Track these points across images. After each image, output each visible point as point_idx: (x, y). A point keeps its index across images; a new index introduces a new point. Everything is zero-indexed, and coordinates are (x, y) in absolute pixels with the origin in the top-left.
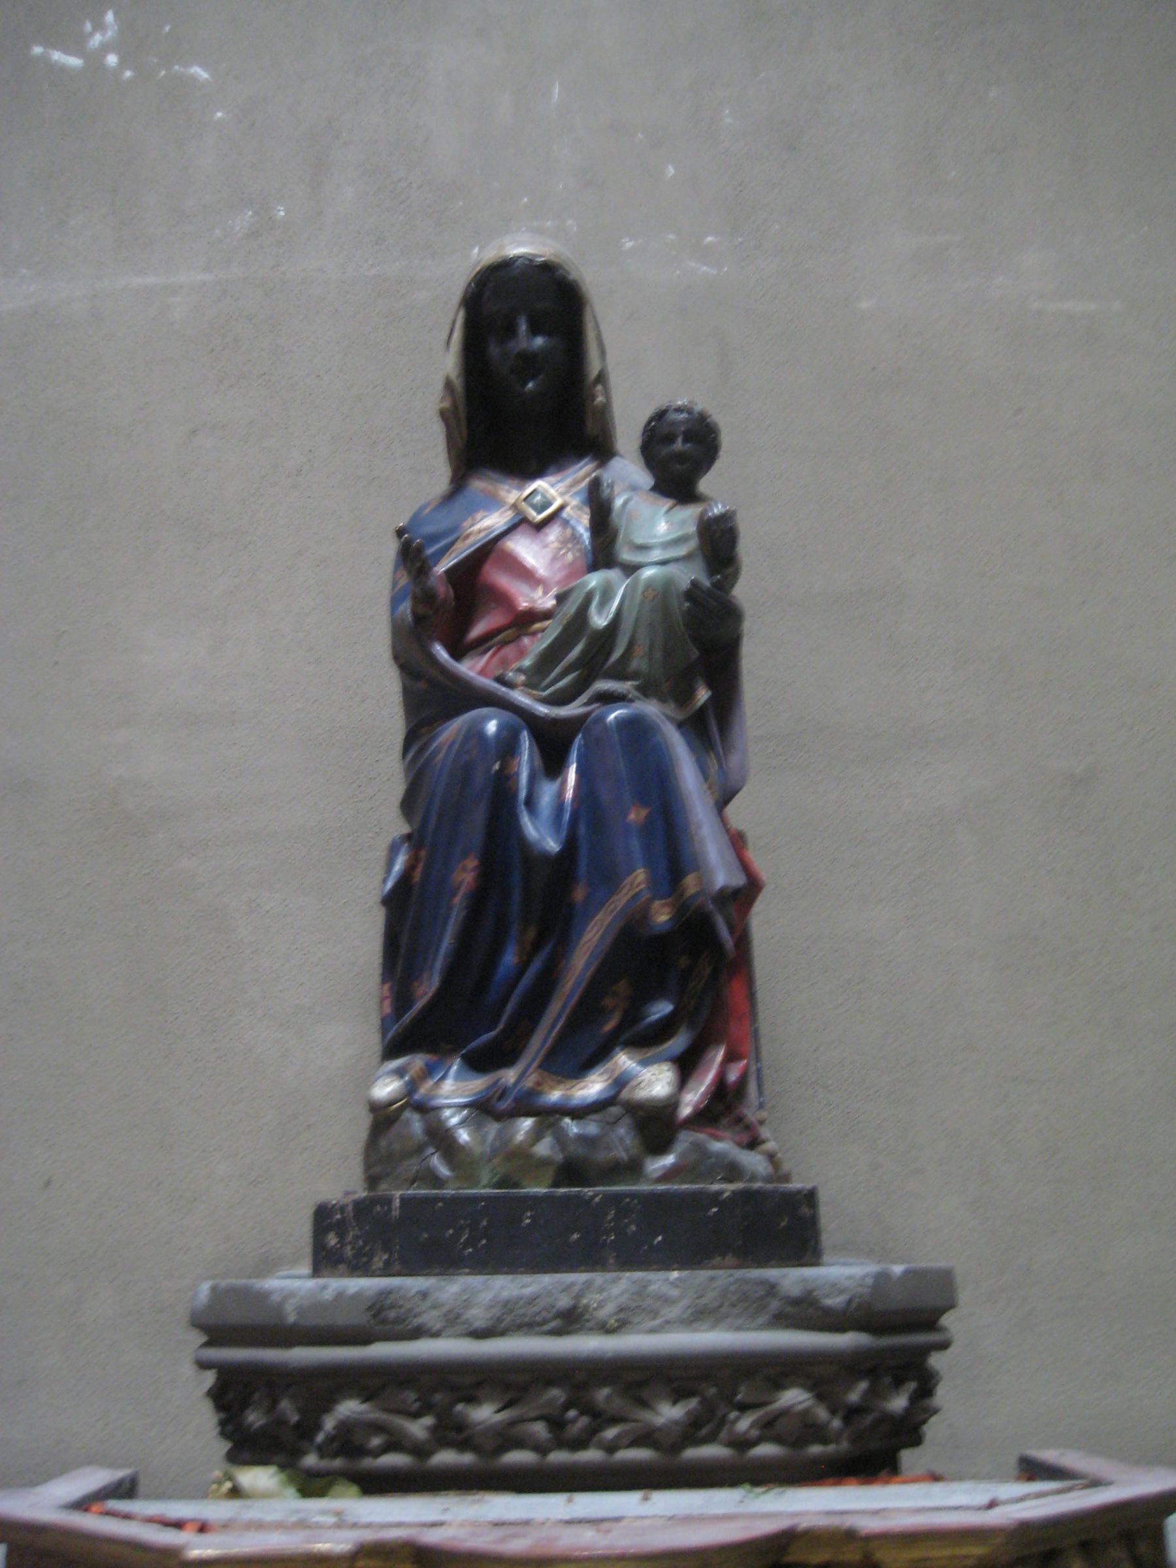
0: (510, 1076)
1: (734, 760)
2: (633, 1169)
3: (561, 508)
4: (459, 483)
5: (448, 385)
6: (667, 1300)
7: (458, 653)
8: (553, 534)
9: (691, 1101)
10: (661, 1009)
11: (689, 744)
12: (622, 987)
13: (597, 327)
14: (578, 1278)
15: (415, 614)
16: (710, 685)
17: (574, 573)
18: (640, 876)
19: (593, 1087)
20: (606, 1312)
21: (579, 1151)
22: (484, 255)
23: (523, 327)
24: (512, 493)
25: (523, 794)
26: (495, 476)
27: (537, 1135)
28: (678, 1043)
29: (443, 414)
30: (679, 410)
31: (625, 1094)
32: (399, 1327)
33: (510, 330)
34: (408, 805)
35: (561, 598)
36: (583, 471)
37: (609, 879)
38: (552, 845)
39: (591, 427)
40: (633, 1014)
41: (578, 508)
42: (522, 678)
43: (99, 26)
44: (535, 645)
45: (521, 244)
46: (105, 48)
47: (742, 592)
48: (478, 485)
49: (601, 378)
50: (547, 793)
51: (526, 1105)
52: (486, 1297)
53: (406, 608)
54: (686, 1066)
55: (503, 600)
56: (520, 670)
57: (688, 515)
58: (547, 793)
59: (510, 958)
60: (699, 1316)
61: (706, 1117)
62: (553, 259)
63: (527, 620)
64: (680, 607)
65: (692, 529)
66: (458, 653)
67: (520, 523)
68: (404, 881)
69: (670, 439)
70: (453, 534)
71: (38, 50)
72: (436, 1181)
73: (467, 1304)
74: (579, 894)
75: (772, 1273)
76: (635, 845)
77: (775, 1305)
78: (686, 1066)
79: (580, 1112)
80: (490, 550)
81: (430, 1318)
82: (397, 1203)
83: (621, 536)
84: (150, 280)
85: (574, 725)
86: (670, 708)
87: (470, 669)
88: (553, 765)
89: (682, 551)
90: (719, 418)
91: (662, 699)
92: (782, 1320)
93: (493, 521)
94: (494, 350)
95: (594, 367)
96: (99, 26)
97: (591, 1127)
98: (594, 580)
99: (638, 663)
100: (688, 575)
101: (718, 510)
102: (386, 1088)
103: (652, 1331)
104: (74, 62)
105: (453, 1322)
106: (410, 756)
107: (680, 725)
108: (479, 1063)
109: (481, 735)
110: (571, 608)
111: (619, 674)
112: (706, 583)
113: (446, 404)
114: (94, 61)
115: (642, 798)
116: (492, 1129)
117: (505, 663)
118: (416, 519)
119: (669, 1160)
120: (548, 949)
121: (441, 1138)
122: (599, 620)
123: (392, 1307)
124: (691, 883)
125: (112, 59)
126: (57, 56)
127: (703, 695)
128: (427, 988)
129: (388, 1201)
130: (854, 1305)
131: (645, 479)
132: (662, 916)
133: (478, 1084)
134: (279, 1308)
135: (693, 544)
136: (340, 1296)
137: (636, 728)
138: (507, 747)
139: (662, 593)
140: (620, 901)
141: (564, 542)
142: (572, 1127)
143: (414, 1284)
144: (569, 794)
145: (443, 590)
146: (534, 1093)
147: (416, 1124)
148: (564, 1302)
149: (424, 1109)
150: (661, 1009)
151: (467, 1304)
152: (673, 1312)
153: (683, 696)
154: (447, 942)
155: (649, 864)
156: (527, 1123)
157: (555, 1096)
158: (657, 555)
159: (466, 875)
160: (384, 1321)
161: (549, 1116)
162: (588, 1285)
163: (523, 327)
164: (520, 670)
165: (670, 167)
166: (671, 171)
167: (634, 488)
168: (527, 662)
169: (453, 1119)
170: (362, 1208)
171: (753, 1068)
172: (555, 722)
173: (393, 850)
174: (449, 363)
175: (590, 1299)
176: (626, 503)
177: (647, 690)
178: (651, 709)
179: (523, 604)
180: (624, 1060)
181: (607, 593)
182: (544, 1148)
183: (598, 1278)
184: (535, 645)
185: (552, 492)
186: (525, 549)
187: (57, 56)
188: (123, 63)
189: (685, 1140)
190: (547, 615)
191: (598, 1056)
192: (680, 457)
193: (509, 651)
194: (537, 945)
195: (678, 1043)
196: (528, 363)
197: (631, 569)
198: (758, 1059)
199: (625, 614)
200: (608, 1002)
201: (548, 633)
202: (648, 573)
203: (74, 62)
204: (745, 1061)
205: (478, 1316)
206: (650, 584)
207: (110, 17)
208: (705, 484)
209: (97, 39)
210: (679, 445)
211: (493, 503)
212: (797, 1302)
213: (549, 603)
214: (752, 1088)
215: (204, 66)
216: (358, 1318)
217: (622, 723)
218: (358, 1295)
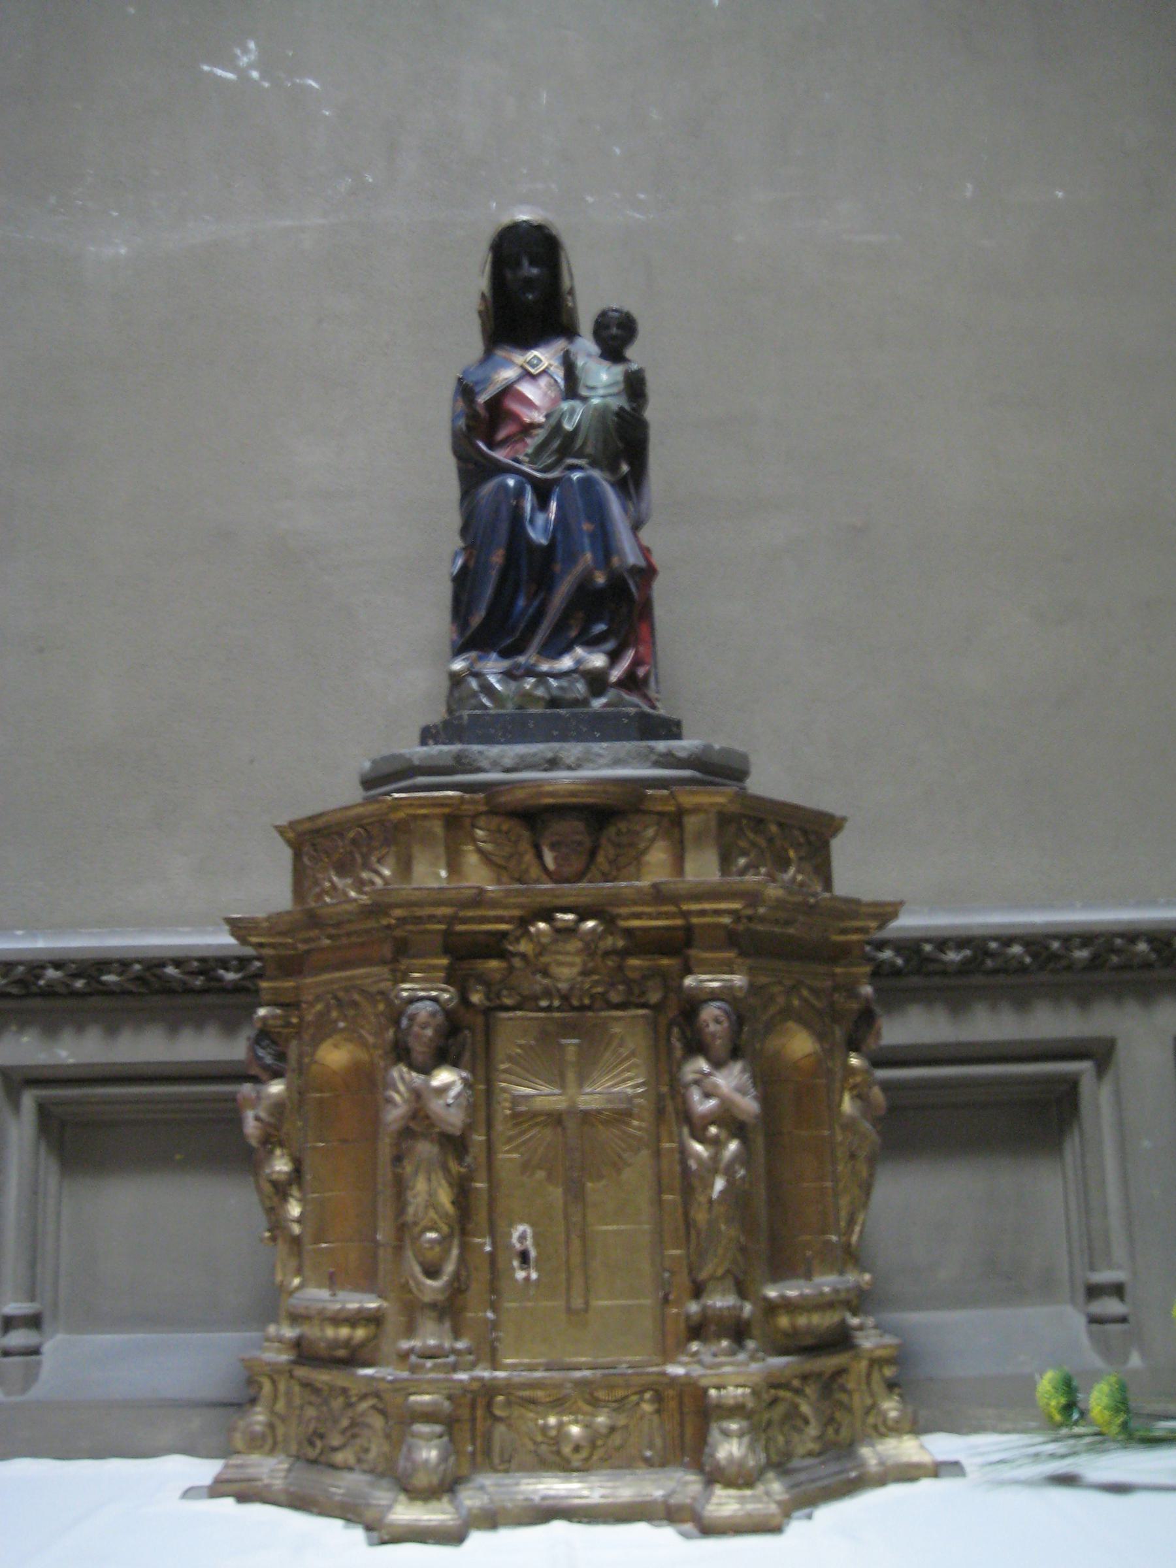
0: (521, 659)
1: (643, 506)
2: (585, 702)
3: (547, 368)
4: (488, 353)
5: (483, 295)
6: (600, 756)
7: (492, 445)
8: (543, 382)
9: (615, 675)
10: (601, 627)
11: (619, 497)
12: (581, 615)
13: (568, 263)
14: (556, 745)
15: (468, 426)
16: (631, 464)
17: (555, 402)
18: (589, 556)
19: (566, 663)
20: (571, 760)
21: (555, 693)
22: (506, 220)
23: (525, 263)
24: (520, 358)
25: (528, 518)
26: (508, 348)
27: (536, 686)
28: (610, 645)
29: (480, 313)
30: (616, 311)
31: (581, 667)
32: (469, 767)
33: (519, 264)
34: (465, 531)
35: (547, 416)
36: (560, 344)
37: (572, 557)
38: (544, 541)
39: (565, 319)
40: (585, 630)
41: (557, 367)
42: (527, 459)
43: (246, 51)
44: (532, 443)
45: (524, 213)
46: (251, 66)
47: (651, 413)
48: (500, 353)
49: (571, 292)
50: (540, 518)
51: (530, 672)
52: (511, 754)
53: (462, 423)
54: (614, 657)
55: (516, 417)
56: (526, 455)
57: (618, 370)
58: (540, 518)
59: (521, 602)
60: (616, 762)
61: (623, 683)
62: (543, 223)
63: (528, 429)
64: (612, 420)
65: (620, 378)
66: (492, 445)
67: (527, 375)
68: (464, 569)
69: (607, 327)
70: (487, 381)
71: (206, 68)
72: (486, 708)
73: (502, 757)
74: (558, 567)
75: (652, 743)
76: (586, 541)
77: (654, 757)
78: (614, 657)
79: (557, 676)
80: (508, 390)
81: (484, 764)
82: (466, 717)
83: (582, 382)
84: (288, 223)
85: (556, 481)
86: (607, 475)
87: (500, 455)
88: (543, 504)
89: (614, 390)
90: (636, 313)
91: (601, 469)
92: (657, 764)
93: (508, 374)
94: (509, 275)
95: (566, 283)
96: (246, 51)
97: (564, 683)
98: (565, 406)
99: (589, 450)
100: (616, 403)
101: (634, 367)
102: (458, 665)
103: (593, 769)
104: (230, 76)
105: (496, 765)
106: (466, 504)
107: (613, 485)
108: (505, 654)
109: (506, 486)
110: (553, 421)
111: (579, 455)
112: (627, 407)
113: (482, 308)
114: (242, 73)
115: (590, 519)
116: (513, 685)
117: (517, 452)
118: (465, 372)
119: (604, 700)
120: (542, 595)
121: (488, 689)
122: (568, 427)
123: (467, 757)
124: (615, 561)
125: (255, 74)
126: (219, 72)
127: (625, 468)
128: (476, 620)
129: (460, 717)
130: (693, 757)
131: (594, 349)
132: (600, 579)
133: (505, 664)
134: (409, 760)
135: (622, 386)
136: (441, 752)
137: (588, 484)
138: (519, 493)
139: (602, 413)
140: (578, 569)
141: (549, 386)
142: (553, 682)
143: (476, 748)
144: (552, 516)
145: (482, 412)
146: (534, 665)
147: (474, 684)
148: (550, 755)
149: (477, 675)
150: (601, 627)
151: (502, 757)
152: (602, 761)
153: (613, 468)
154: (489, 592)
155: (594, 552)
156: (532, 680)
157: (545, 667)
158: (601, 392)
159: (497, 558)
160: (463, 764)
161: (542, 677)
162: (561, 749)
163: (525, 263)
164: (526, 455)
165: (614, 148)
166: (618, 151)
167: (589, 355)
168: (530, 450)
169: (492, 680)
170: (446, 724)
171: (653, 671)
172: (546, 481)
173: (456, 555)
174: (481, 282)
175: (563, 754)
176: (585, 364)
177: (594, 464)
178: (596, 474)
179: (527, 420)
180: (579, 651)
181: (572, 412)
182: (540, 692)
183: (566, 745)
184: (532, 443)
185: (542, 358)
186: (528, 390)
187: (219, 72)
188: (263, 77)
189: (612, 693)
190: (540, 426)
191: (567, 649)
192: (615, 338)
193: (519, 446)
194: (536, 594)
195: (610, 645)
196: (529, 283)
197: (585, 399)
198: (656, 667)
199: (583, 421)
200: (572, 622)
201: (540, 435)
202: (596, 401)
203: (230, 76)
204: (647, 668)
205: (508, 762)
206: (596, 408)
207: (252, 45)
208: (629, 353)
209: (244, 60)
210: (614, 331)
211: (509, 363)
212: (661, 755)
213: (542, 419)
214: (652, 679)
215: (316, 80)
216: (450, 762)
217: (580, 480)
218: (449, 752)
